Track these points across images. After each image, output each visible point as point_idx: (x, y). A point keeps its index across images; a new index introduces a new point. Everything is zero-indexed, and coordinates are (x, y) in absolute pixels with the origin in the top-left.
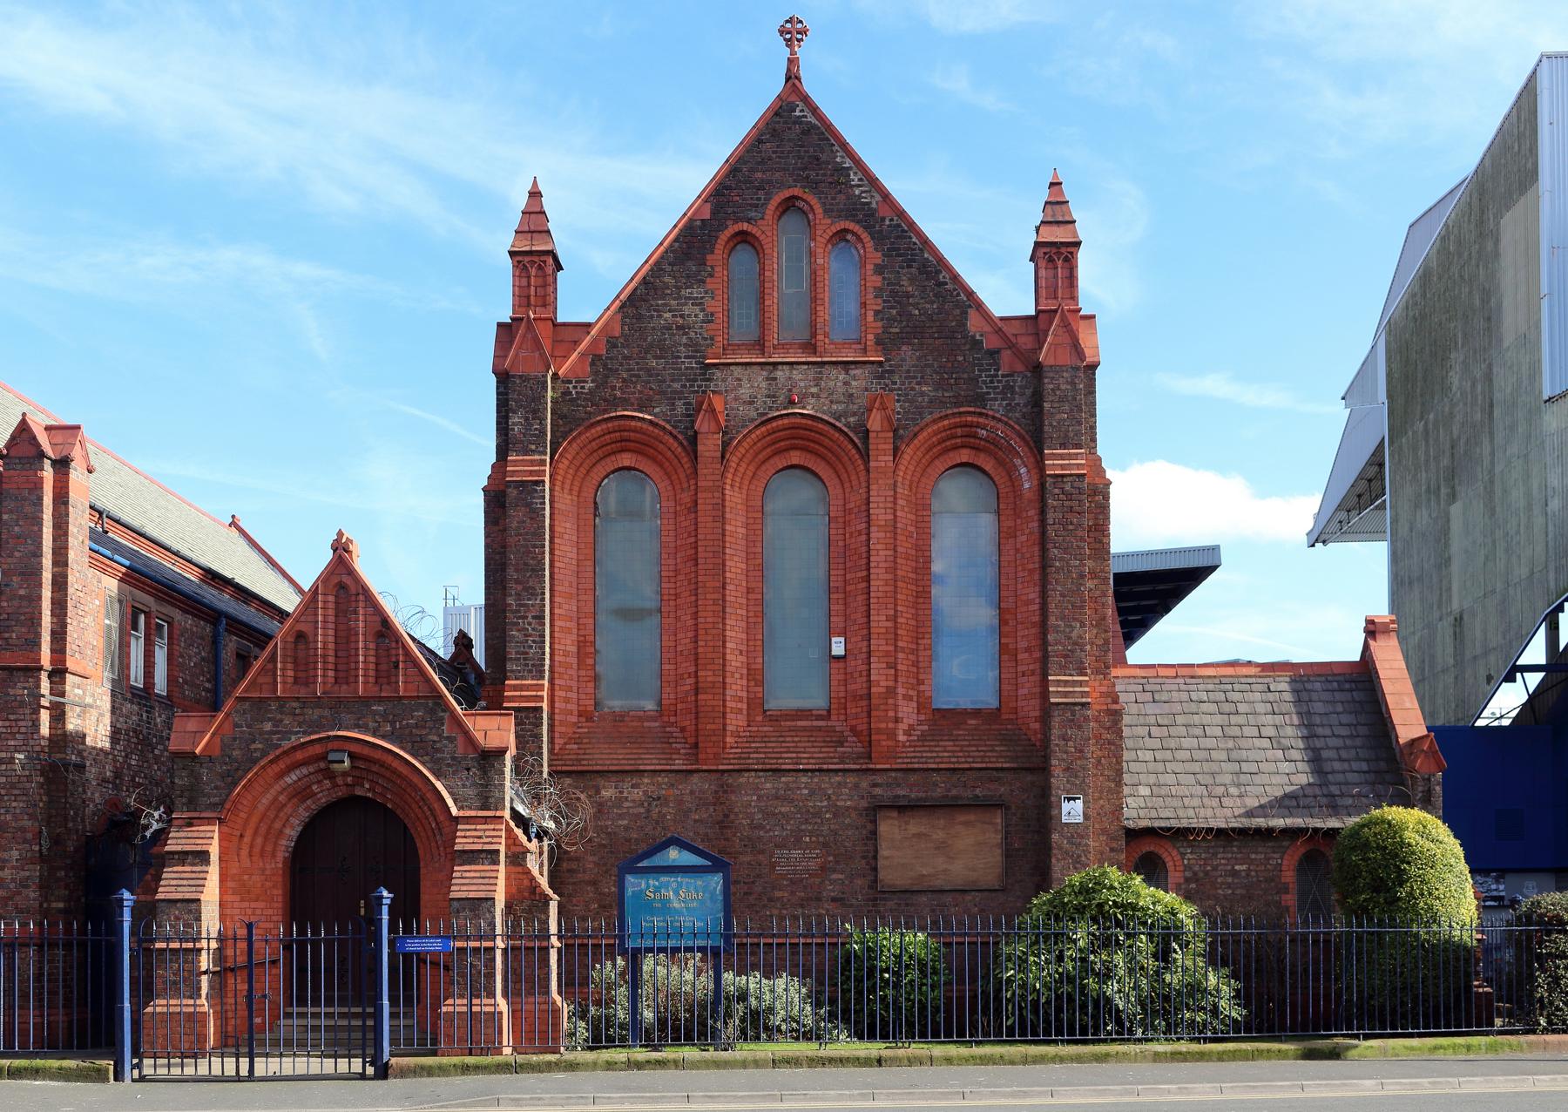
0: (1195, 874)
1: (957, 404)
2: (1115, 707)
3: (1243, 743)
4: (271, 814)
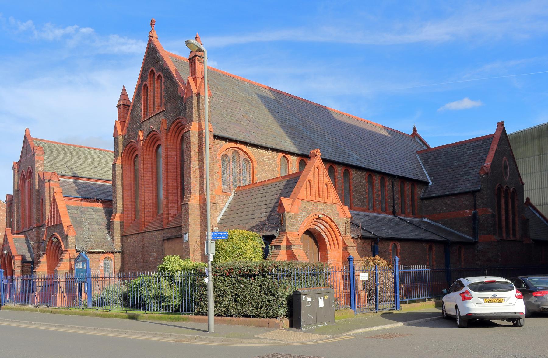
4: (54, 252)
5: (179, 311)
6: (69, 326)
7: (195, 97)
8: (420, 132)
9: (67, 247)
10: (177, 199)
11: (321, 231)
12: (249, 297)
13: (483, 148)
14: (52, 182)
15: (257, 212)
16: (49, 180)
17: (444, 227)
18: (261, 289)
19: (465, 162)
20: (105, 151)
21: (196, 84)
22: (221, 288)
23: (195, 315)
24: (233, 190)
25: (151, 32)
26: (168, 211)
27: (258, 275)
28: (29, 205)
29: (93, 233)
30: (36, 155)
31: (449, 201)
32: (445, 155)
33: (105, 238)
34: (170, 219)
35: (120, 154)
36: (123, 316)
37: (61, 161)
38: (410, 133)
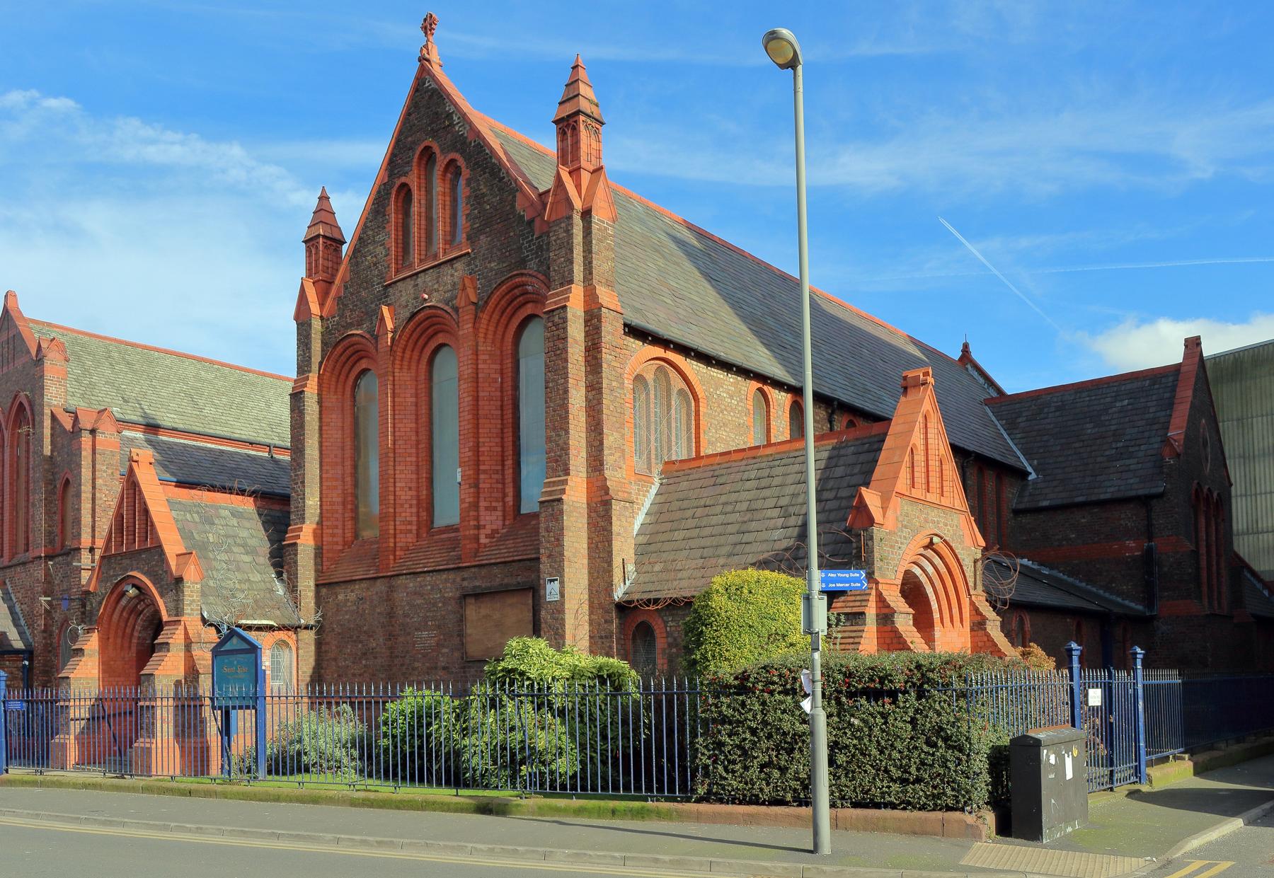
0: (675, 639)
1: (510, 271)
2: (607, 498)
3: (759, 515)
4: (122, 624)
5: (574, 788)
6: (329, 836)
7: (577, 219)
8: (976, 355)
9: (178, 611)
10: (504, 489)
11: (923, 579)
12: (874, 752)
13: (1154, 397)
14: (99, 437)
15: (753, 525)
16: (93, 432)
17: (1071, 580)
18: (914, 729)
19: (1113, 428)
20: (211, 362)
21: (578, 187)
22: (786, 727)
23: (699, 801)
24: (657, 468)
25: (426, 46)
26: (477, 518)
27: (905, 692)
28: (11, 499)
29: (239, 576)
30: (47, 364)
31: (1083, 519)
32: (1058, 409)
33: (271, 591)
34: (483, 540)
35: (315, 367)
36: (448, 804)
37: (107, 383)
38: (956, 354)
